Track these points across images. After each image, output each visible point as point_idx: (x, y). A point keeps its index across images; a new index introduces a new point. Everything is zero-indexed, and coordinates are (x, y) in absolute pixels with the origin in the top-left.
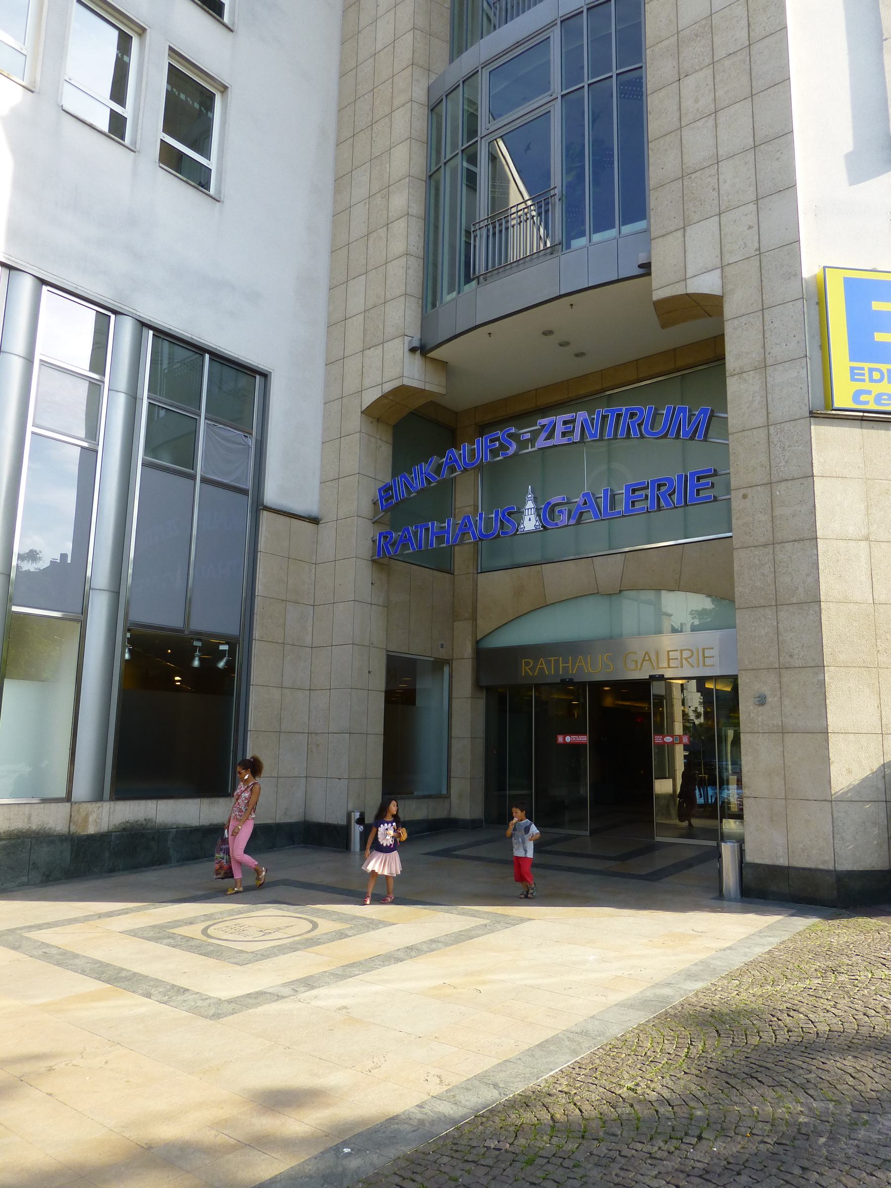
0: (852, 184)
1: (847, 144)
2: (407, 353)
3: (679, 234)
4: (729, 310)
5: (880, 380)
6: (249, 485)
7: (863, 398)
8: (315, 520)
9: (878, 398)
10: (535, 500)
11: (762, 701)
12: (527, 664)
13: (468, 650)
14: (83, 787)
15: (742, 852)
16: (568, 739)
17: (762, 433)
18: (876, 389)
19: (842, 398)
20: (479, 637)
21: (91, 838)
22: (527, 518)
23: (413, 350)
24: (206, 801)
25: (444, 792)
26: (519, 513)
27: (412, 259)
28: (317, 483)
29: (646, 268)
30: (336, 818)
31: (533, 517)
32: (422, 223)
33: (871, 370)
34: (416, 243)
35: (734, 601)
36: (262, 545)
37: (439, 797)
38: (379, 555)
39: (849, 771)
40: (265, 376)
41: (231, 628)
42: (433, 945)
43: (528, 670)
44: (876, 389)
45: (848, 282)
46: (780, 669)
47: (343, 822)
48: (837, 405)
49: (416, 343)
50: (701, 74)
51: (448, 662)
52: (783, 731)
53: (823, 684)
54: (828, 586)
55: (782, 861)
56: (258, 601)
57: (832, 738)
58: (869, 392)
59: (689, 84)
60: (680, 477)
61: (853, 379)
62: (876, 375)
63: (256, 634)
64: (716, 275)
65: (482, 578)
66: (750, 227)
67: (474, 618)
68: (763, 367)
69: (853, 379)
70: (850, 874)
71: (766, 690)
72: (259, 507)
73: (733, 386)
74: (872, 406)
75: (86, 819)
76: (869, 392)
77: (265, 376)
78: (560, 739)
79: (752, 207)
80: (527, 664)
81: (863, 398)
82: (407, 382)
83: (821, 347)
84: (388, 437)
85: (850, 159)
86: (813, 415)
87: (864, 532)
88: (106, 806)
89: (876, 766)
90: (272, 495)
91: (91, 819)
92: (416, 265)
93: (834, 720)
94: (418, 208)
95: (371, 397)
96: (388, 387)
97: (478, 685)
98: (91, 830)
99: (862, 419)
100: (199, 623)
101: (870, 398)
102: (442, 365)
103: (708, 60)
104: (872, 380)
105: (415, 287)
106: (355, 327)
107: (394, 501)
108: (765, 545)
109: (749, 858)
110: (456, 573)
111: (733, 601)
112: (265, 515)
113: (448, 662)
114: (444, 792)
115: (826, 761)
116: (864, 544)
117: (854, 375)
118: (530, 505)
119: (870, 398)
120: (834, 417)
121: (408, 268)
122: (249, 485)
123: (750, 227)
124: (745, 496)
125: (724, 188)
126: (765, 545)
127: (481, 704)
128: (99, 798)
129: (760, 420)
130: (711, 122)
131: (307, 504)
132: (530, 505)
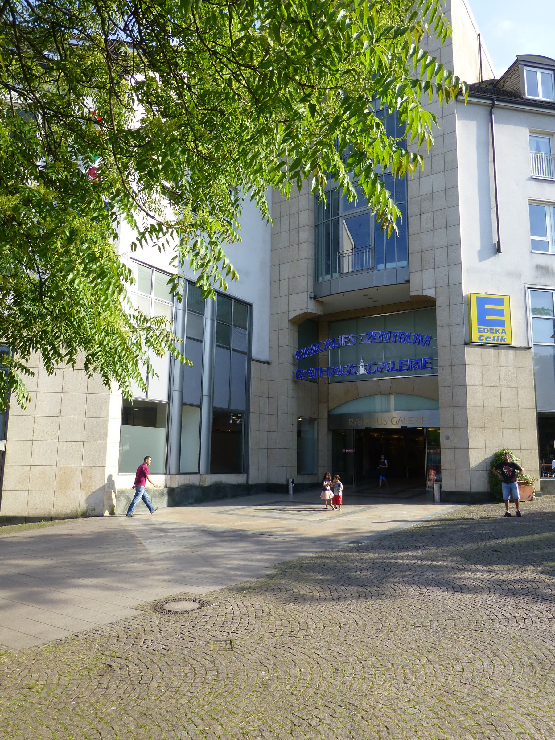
0: (480, 262)
1: (479, 248)
2: (309, 299)
3: (420, 272)
4: (438, 303)
5: (487, 332)
6: (246, 350)
7: (482, 338)
8: (268, 363)
9: (486, 339)
10: (364, 363)
11: (447, 438)
12: (351, 421)
13: (325, 415)
14: (203, 470)
15: (441, 487)
16: (347, 451)
17: (449, 348)
18: (486, 335)
19: (475, 339)
20: (330, 409)
21: (207, 487)
22: (361, 369)
23: (311, 298)
24: (237, 475)
25: (316, 472)
26: (358, 367)
27: (310, 260)
28: (268, 348)
29: (408, 282)
30: (282, 481)
31: (363, 369)
32: (313, 245)
33: (484, 329)
34: (311, 253)
35: (438, 401)
36: (252, 374)
37: (313, 474)
38: (297, 378)
39: (475, 461)
40: (251, 305)
41: (241, 408)
42: (351, 513)
43: (352, 424)
44: (486, 335)
45: (478, 298)
46: (454, 428)
47: (284, 482)
48: (473, 341)
49: (313, 295)
50: (428, 214)
51: (317, 419)
52: (455, 448)
53: (467, 433)
54: (470, 401)
55: (454, 490)
56: (251, 397)
57: (470, 450)
58: (484, 336)
59: (424, 217)
60: (419, 359)
61: (479, 332)
62: (486, 331)
63: (251, 410)
64: (433, 290)
65: (330, 385)
66: (445, 275)
67: (327, 402)
68: (449, 325)
69: (479, 332)
70: (476, 493)
71: (449, 434)
72: (250, 359)
73: (439, 330)
74: (485, 341)
75: (205, 481)
76: (484, 336)
77: (251, 305)
78: (344, 451)
79: (446, 268)
80: (351, 421)
81: (482, 338)
82: (309, 311)
83: (468, 320)
84: (297, 330)
85: (479, 252)
86: (465, 344)
87: (481, 383)
88: (210, 476)
89: (483, 459)
90: (254, 355)
91: (206, 480)
92: (311, 262)
93: (471, 444)
94: (311, 239)
95: (293, 315)
96: (301, 312)
97: (329, 429)
98: (207, 485)
99: (481, 345)
100: (233, 407)
101: (484, 338)
102: (321, 303)
103: (431, 210)
104: (485, 332)
105: (311, 272)
106: (284, 284)
107: (303, 358)
108: (450, 386)
109: (444, 489)
110: (319, 382)
111: (437, 401)
112: (253, 363)
113: (317, 419)
114: (316, 472)
115: (468, 458)
116: (481, 387)
117: (479, 330)
118: (362, 364)
119: (484, 338)
120: (472, 345)
121: (308, 264)
122: (246, 350)
123: (445, 275)
124: (443, 369)
125: (436, 259)
126: (450, 386)
127: (330, 437)
128: (207, 473)
129: (448, 343)
130: (432, 233)
131: (264, 357)
132: (362, 364)
